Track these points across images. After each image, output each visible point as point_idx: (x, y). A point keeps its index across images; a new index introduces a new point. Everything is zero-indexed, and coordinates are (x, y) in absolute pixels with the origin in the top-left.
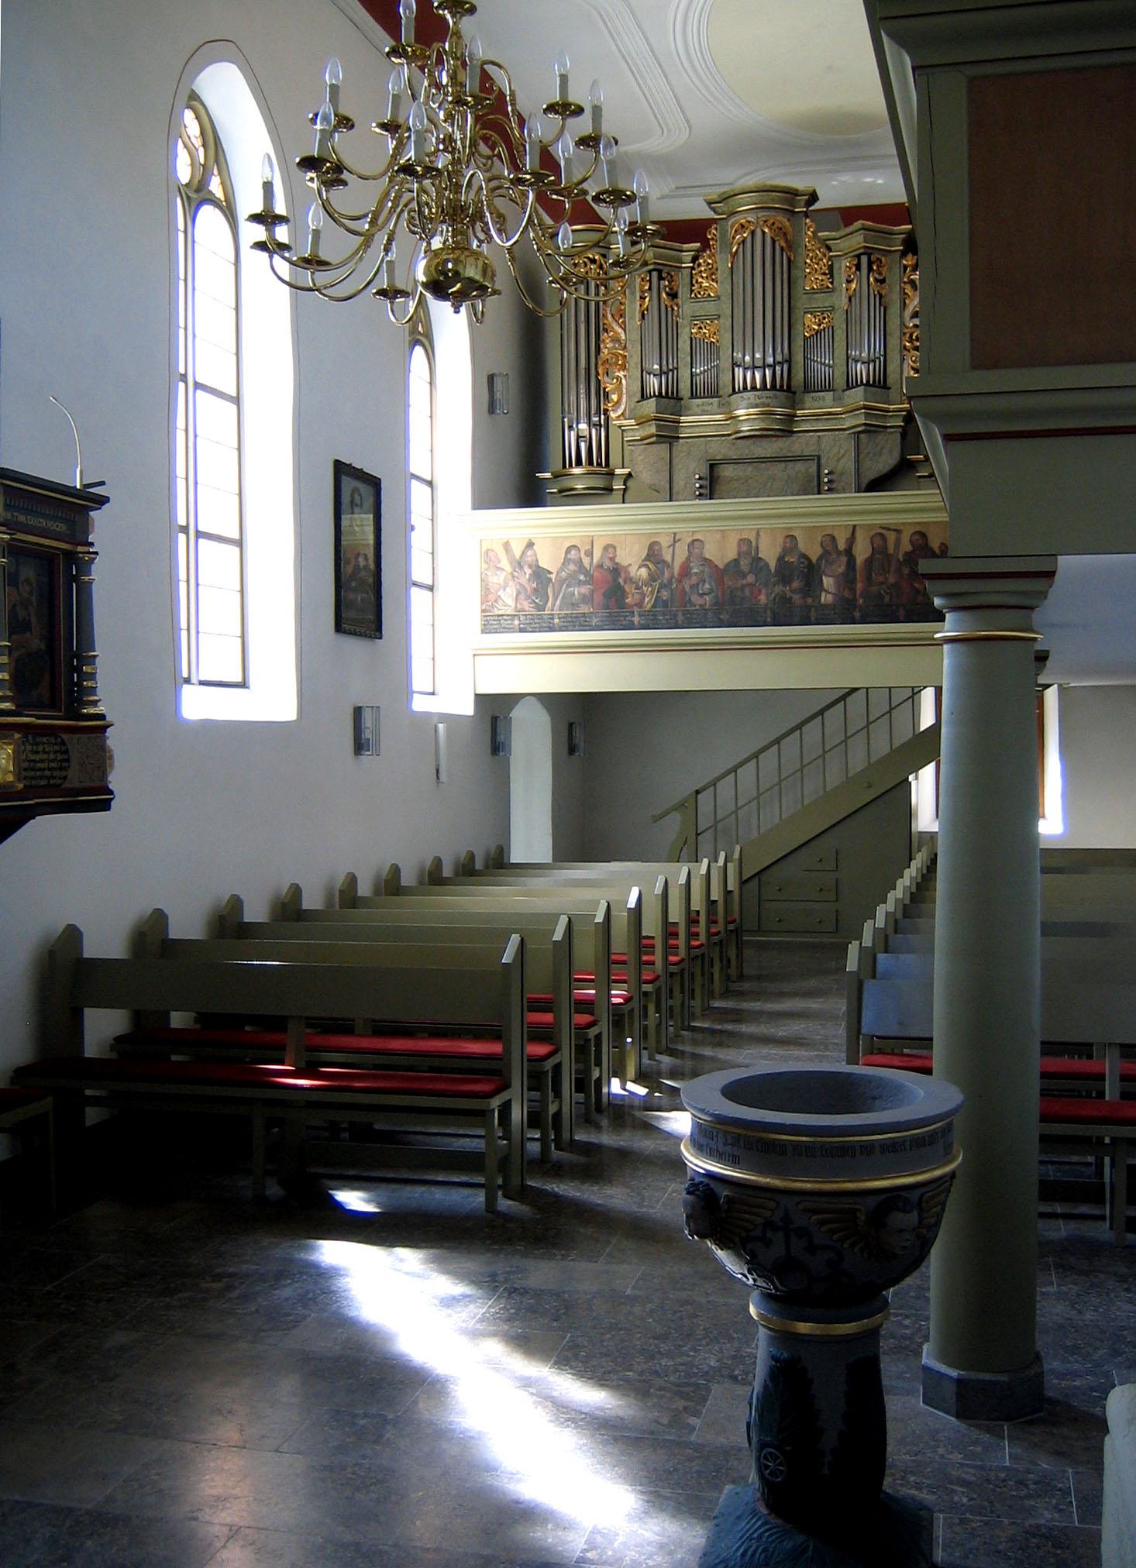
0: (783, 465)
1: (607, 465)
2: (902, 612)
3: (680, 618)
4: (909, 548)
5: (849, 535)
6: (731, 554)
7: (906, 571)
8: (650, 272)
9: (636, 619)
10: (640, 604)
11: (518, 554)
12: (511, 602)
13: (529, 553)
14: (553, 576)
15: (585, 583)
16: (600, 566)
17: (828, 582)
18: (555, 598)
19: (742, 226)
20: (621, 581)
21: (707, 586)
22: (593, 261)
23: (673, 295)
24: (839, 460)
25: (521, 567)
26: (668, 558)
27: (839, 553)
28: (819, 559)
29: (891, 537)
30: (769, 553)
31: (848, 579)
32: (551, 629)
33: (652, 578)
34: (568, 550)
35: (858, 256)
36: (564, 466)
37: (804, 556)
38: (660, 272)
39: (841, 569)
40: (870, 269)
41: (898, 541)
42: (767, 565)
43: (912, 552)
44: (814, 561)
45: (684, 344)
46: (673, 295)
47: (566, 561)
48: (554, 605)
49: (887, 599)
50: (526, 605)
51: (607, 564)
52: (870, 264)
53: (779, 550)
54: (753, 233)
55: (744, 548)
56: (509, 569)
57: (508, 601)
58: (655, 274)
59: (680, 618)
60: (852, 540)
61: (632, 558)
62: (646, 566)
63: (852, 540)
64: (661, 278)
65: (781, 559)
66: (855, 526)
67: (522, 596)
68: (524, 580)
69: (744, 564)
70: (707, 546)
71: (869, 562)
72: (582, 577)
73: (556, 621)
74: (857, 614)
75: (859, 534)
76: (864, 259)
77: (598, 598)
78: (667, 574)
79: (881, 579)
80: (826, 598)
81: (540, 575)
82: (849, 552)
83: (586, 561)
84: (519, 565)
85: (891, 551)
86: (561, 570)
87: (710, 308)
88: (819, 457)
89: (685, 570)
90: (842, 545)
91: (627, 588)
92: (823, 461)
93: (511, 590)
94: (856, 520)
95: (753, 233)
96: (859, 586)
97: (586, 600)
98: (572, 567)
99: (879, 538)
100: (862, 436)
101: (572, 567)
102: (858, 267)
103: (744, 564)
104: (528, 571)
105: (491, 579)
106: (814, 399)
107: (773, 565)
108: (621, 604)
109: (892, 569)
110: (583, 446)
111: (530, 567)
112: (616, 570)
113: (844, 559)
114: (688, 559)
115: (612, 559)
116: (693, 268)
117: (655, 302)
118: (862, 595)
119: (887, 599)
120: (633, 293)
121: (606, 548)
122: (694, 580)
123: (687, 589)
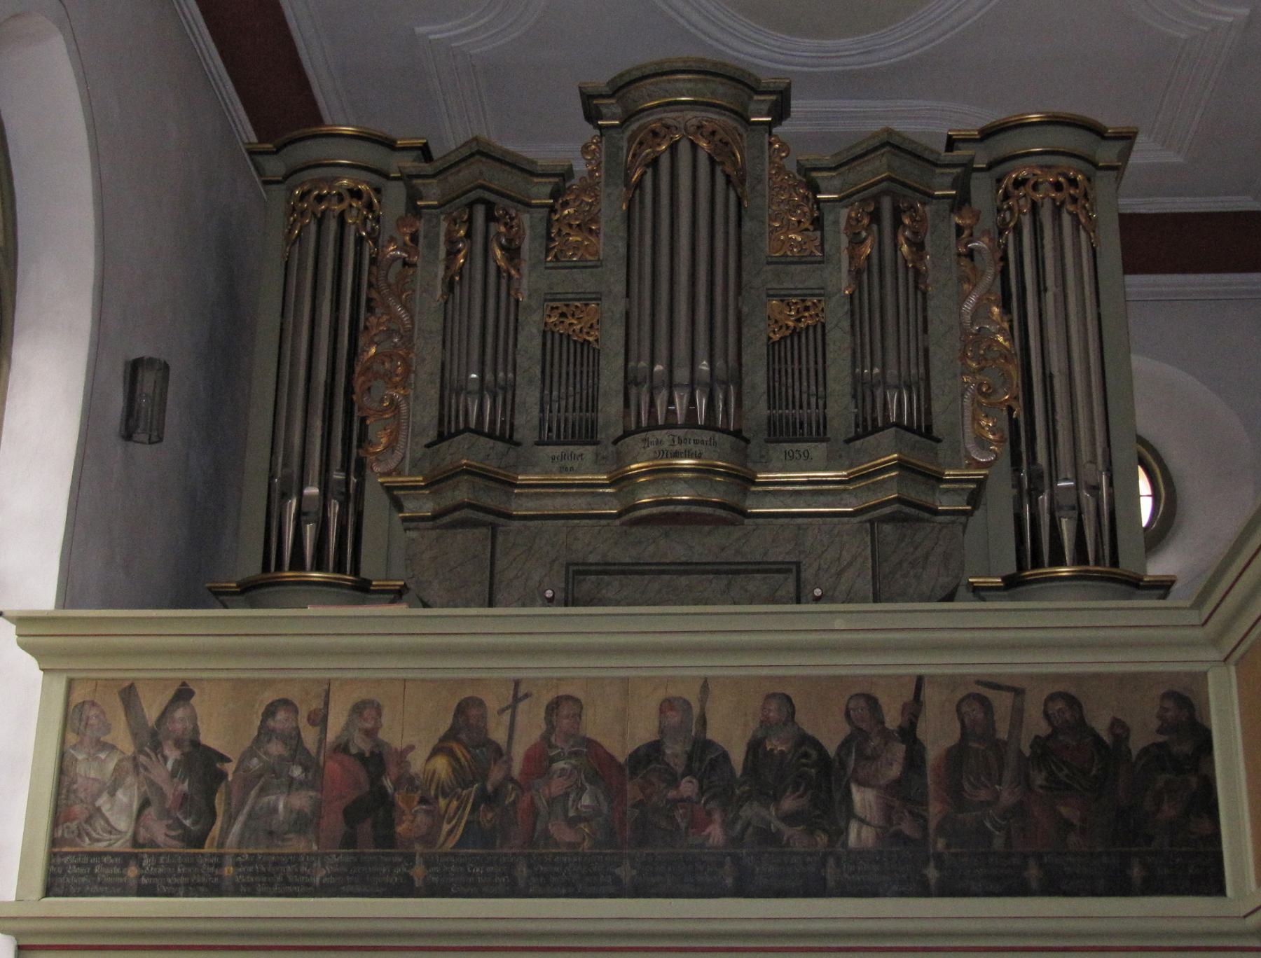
0: (724, 580)
1: (356, 570)
2: (1033, 872)
3: (522, 871)
4: (1043, 729)
5: (908, 695)
6: (644, 731)
7: (1039, 779)
8: (471, 205)
9: (418, 872)
10: (429, 838)
11: (152, 713)
12: (123, 824)
13: (180, 713)
14: (230, 768)
15: (303, 785)
16: (342, 748)
17: (863, 798)
18: (231, 819)
19: (655, 134)
20: (388, 784)
21: (586, 800)
22: (356, 194)
23: (512, 252)
24: (839, 574)
25: (157, 747)
26: (498, 734)
27: (886, 734)
28: (845, 745)
29: (1002, 703)
30: (731, 734)
31: (904, 794)
32: (215, 890)
33: (462, 777)
34: (270, 711)
35: (876, 198)
36: (266, 567)
37: (805, 740)
38: (490, 206)
39: (895, 771)
40: (897, 223)
41: (1018, 714)
42: (725, 756)
43: (1049, 737)
44: (832, 749)
45: (530, 341)
46: (512, 252)
47: (265, 733)
48: (225, 832)
49: (998, 843)
50: (158, 831)
51: (360, 744)
52: (897, 214)
53: (753, 725)
54: (673, 148)
55: (674, 718)
56: (126, 745)
57: (118, 814)
58: (480, 212)
59: (522, 871)
60: (915, 707)
61: (413, 736)
62: (451, 754)
63: (915, 707)
64: (490, 218)
65: (755, 747)
66: (920, 680)
67: (151, 811)
68: (160, 773)
69: (675, 751)
70: (589, 714)
71: (956, 757)
72: (297, 772)
73: (228, 870)
74: (932, 873)
75: (927, 691)
76: (886, 204)
77: (334, 822)
78: (496, 775)
79: (983, 795)
80: (858, 836)
81: (203, 765)
82: (908, 734)
83: (309, 737)
84: (150, 740)
85: (1002, 733)
86: (250, 753)
87: (584, 281)
88: (798, 564)
89: (540, 761)
90: (893, 719)
91: (399, 799)
92: (807, 574)
93: (127, 798)
94: (927, 665)
95: (673, 148)
96: (934, 810)
97: (303, 823)
98: (276, 748)
99: (977, 699)
100: (887, 528)
101: (276, 748)
102: (875, 217)
103: (675, 751)
104: (173, 754)
105: (81, 769)
106: (789, 456)
107: (738, 756)
108: (386, 837)
109: (1008, 775)
110: (309, 530)
111: (178, 744)
112: (375, 761)
113: (899, 750)
114: (546, 738)
115: (371, 734)
116: (552, 209)
117: (479, 263)
118: (940, 829)
119: (998, 843)
120: (432, 246)
121: (358, 709)
122: (557, 786)
123: (542, 804)
